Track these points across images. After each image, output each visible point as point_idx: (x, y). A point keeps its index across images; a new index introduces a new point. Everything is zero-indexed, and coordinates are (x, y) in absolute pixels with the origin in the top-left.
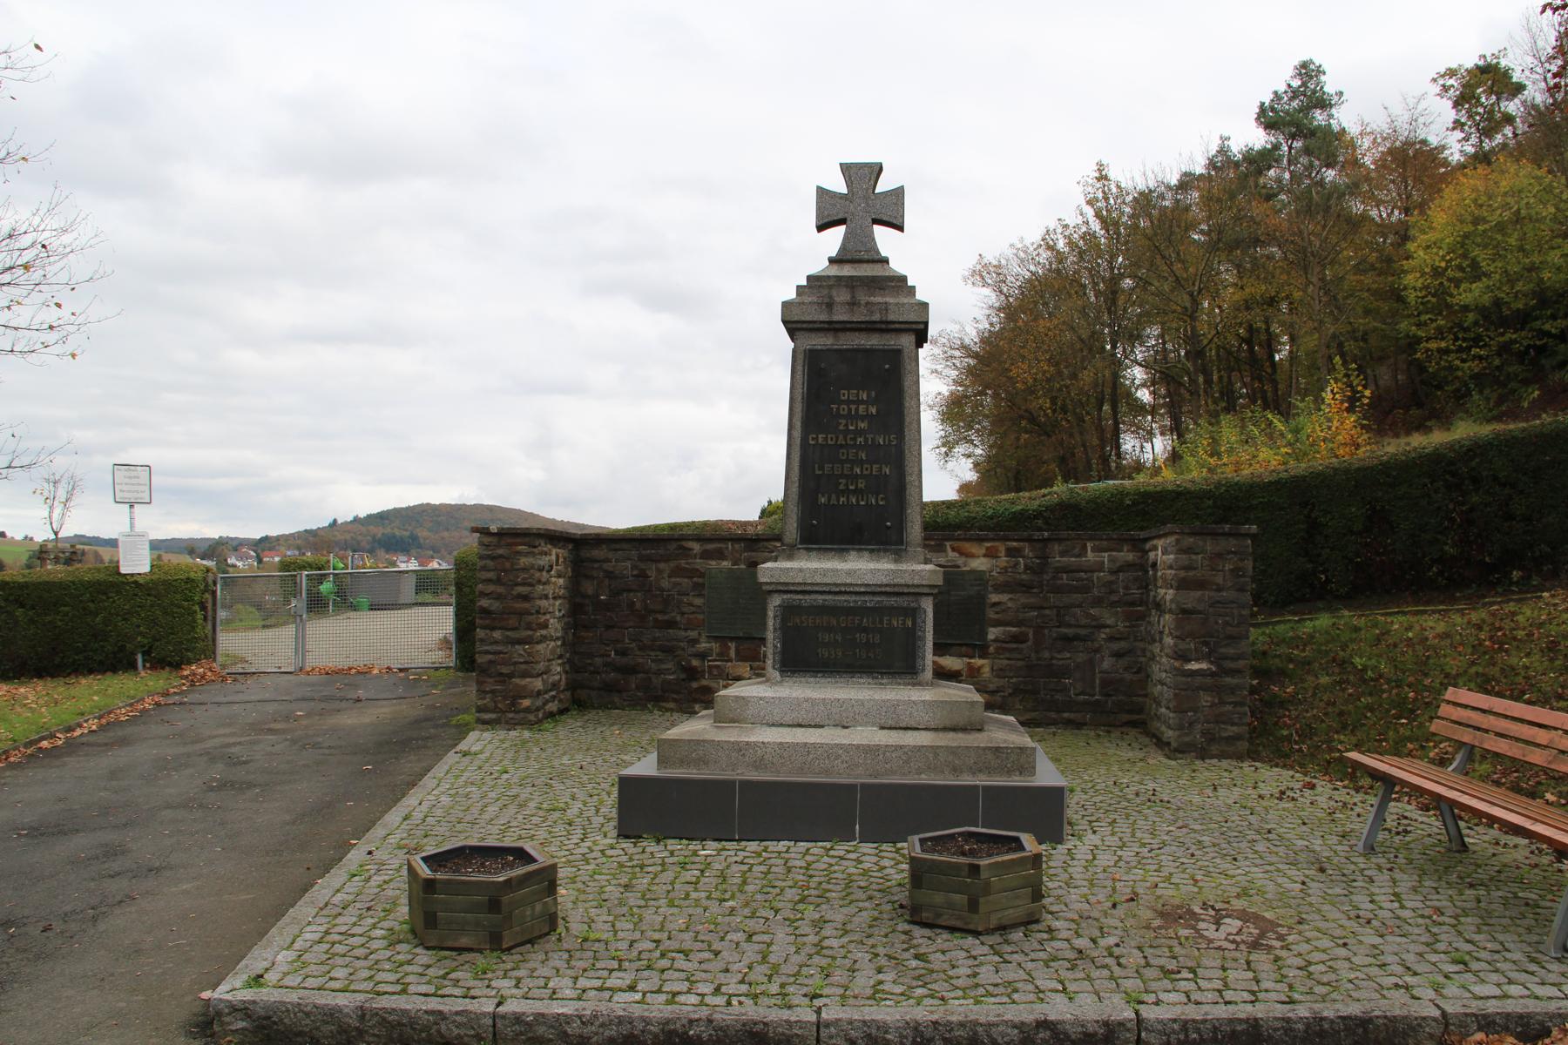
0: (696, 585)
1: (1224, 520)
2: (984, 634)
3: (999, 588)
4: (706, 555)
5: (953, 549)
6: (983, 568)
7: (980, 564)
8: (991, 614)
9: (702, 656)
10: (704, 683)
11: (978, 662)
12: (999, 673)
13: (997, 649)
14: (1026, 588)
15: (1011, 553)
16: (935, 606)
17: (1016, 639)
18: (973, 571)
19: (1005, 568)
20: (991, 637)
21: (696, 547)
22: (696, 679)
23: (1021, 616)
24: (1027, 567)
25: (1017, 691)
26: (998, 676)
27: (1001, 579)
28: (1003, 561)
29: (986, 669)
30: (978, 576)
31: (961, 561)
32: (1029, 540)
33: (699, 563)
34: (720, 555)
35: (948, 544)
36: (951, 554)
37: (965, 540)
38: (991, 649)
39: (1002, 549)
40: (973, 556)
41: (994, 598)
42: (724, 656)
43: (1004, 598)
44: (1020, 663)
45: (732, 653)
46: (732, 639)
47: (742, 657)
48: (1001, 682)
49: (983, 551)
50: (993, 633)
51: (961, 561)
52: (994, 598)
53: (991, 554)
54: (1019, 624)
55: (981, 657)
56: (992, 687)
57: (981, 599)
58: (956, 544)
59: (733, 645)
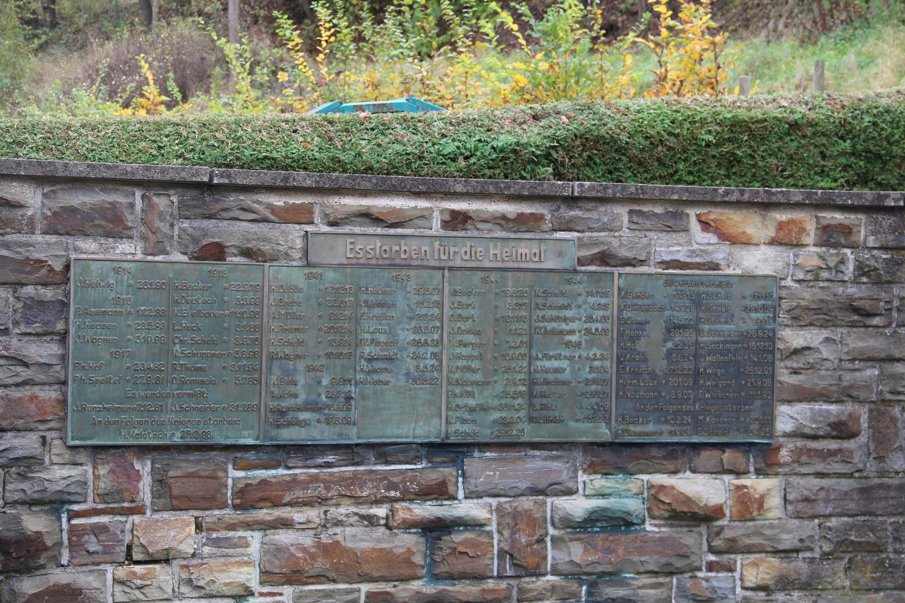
0: (35, 306)
1: (864, 180)
2: (768, 420)
3: (802, 317)
4: (65, 223)
5: (706, 225)
6: (766, 270)
7: (760, 260)
8: (784, 376)
9: (54, 503)
10: (59, 577)
11: (757, 484)
12: (802, 507)
13: (797, 454)
14: (860, 314)
15: (830, 237)
16: (871, 411)
17: (842, 430)
18: (748, 278)
19: (815, 273)
20: (783, 425)
21: (32, 198)
22: (28, 569)
23: (848, 377)
24: (862, 270)
25: (843, 546)
26: (798, 516)
27: (807, 295)
28: (811, 254)
29: (774, 501)
30: (765, 293)
31: (721, 253)
32: (874, 209)
33: (45, 247)
34: (112, 225)
35: (692, 212)
36: (701, 237)
37: (739, 204)
38: (784, 455)
39: (811, 226)
40: (747, 242)
41: (794, 338)
42: (121, 501)
43: (811, 337)
44: (845, 484)
45: (145, 489)
46: (144, 450)
47: (170, 498)
48: (810, 528)
49: (771, 232)
50: (788, 417)
51: (721, 253)
52: (794, 338)
53: (785, 240)
54: (846, 394)
55: (759, 472)
56: (788, 541)
57: (764, 346)
58: (715, 214)
59: (144, 467)
